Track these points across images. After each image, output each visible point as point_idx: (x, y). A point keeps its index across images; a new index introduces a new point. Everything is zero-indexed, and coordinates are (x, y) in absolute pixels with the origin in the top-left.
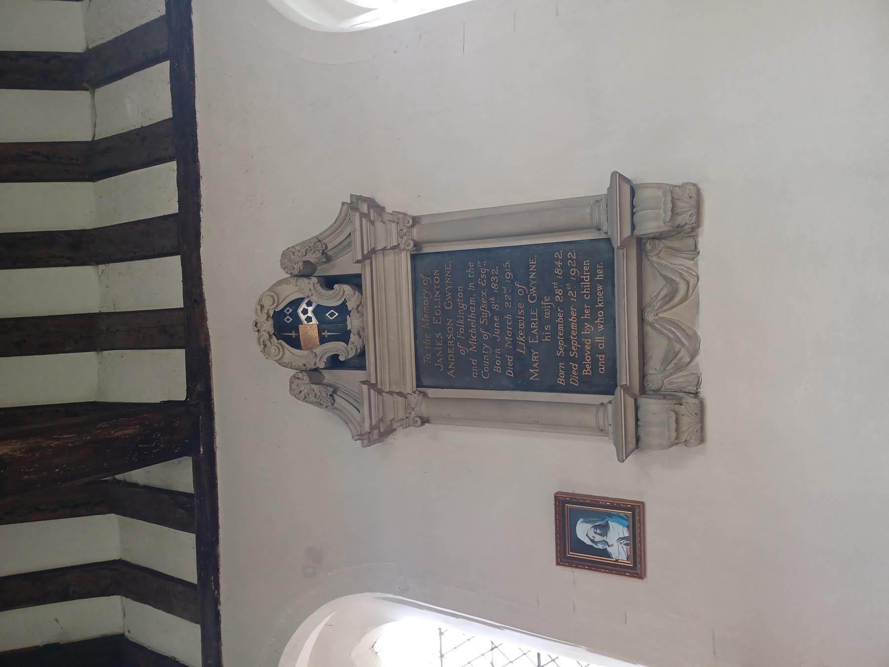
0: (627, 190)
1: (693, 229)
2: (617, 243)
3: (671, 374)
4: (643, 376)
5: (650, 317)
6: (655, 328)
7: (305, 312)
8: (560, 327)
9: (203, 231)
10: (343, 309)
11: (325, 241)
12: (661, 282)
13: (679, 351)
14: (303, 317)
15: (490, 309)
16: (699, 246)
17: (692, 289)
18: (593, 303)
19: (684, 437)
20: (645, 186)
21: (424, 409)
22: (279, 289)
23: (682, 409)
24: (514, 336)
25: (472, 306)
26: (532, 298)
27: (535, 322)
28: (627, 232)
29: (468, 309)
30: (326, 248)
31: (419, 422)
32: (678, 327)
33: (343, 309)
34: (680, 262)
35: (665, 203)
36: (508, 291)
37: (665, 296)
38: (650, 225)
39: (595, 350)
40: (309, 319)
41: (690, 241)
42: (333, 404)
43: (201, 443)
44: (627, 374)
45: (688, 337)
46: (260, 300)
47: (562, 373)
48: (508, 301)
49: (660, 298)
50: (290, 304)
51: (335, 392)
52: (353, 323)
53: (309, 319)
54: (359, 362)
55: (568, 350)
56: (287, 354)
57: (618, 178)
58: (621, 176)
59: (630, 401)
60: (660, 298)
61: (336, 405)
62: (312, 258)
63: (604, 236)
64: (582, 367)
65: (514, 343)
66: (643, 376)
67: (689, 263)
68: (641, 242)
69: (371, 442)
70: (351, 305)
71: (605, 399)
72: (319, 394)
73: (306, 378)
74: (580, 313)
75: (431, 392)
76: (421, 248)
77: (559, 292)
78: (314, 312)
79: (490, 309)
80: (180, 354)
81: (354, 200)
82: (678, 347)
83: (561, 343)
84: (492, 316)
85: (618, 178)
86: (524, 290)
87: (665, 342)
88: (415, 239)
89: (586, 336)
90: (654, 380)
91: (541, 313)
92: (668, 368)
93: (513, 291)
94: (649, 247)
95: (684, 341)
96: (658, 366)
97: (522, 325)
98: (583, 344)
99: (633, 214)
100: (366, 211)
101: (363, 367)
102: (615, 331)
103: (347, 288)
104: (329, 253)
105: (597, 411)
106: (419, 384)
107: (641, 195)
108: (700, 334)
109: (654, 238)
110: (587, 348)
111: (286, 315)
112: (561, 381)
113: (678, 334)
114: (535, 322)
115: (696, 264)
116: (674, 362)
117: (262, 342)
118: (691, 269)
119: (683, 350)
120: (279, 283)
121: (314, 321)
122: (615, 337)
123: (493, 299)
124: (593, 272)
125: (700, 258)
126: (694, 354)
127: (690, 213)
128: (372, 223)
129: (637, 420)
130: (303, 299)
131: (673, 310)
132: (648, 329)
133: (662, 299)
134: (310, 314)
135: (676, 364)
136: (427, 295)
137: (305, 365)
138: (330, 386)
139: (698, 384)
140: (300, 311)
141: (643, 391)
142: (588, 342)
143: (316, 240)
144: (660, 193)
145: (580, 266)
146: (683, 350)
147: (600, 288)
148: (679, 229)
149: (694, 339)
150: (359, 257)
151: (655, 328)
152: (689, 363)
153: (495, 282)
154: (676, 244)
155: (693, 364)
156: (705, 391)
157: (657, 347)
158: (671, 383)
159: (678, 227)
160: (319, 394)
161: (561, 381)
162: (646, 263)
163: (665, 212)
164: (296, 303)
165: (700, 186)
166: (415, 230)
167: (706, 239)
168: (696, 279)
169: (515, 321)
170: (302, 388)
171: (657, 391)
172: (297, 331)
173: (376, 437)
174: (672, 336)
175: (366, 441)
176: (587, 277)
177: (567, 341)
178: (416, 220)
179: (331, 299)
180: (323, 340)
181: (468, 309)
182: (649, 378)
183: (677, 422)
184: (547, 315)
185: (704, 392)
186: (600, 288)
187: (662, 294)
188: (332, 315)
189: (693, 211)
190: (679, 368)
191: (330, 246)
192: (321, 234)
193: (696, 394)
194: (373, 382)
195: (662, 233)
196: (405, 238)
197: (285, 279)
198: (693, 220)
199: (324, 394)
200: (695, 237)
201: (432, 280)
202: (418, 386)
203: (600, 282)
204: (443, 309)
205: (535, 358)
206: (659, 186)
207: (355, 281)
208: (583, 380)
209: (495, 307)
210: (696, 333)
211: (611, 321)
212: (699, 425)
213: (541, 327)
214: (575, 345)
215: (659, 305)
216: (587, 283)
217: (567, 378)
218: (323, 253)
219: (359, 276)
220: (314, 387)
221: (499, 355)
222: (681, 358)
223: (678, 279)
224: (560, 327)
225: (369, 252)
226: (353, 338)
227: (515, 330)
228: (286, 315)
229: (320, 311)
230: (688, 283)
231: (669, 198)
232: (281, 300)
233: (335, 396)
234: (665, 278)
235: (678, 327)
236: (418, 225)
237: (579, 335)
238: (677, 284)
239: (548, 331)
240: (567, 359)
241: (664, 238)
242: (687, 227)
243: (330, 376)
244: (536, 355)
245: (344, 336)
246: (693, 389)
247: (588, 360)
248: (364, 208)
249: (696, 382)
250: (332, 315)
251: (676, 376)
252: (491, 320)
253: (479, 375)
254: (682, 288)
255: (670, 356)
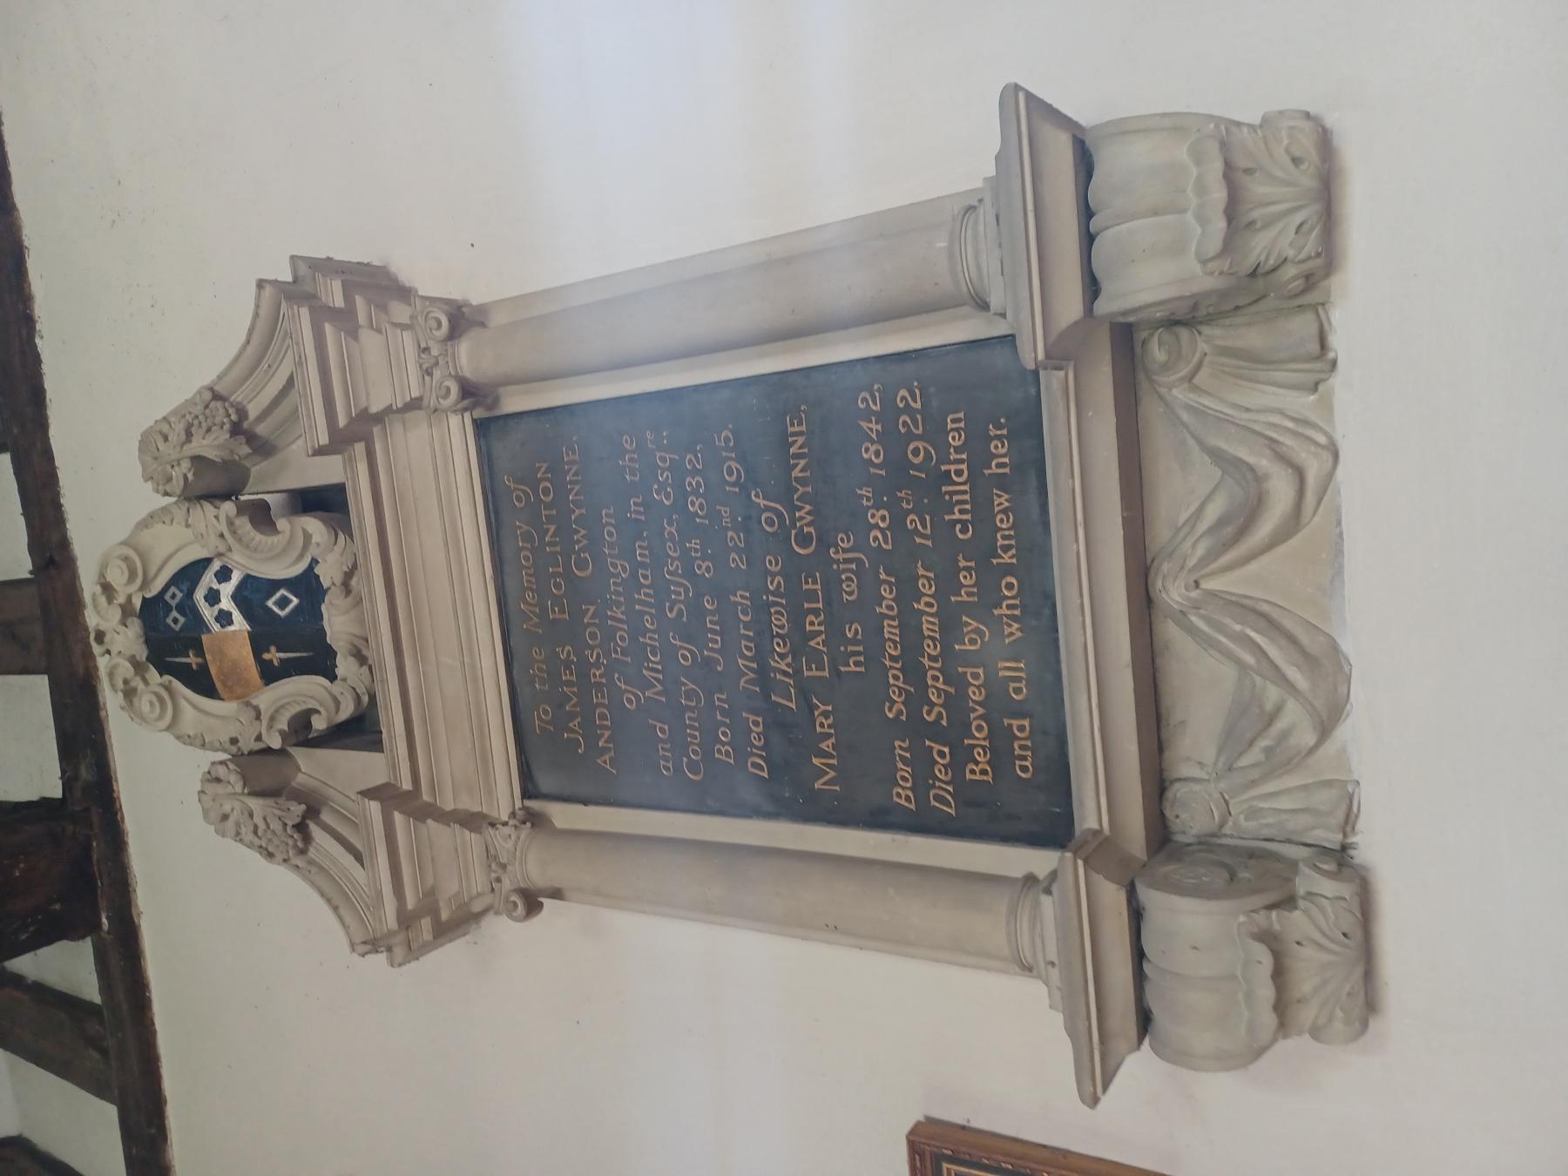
0: (1060, 157)
1: (1311, 281)
2: (1032, 351)
3: (1254, 783)
4: (1158, 784)
5: (1172, 592)
6: (1192, 630)
7: (213, 597)
8: (890, 630)
9: (49, 384)
10: (308, 586)
11: (237, 397)
12: (1204, 474)
13: (1279, 709)
14: (208, 613)
15: (690, 574)
16: (1334, 340)
17: (1312, 497)
18: (984, 552)
19: (1307, 1015)
20: (1123, 129)
21: (537, 866)
22: (146, 537)
23: (1296, 923)
24: (761, 657)
25: (643, 565)
26: (804, 540)
27: (816, 612)
28: (1070, 306)
29: (634, 575)
30: (242, 413)
31: (521, 910)
32: (1271, 625)
33: (308, 586)
34: (1273, 400)
35: (1201, 189)
36: (734, 520)
37: (1221, 523)
38: (1146, 278)
39: (998, 704)
40: (224, 618)
41: (1302, 325)
42: (303, 852)
43: (103, 904)
44: (1103, 796)
45: (1308, 660)
46: (102, 575)
47: (904, 771)
48: (736, 548)
49: (1202, 527)
50: (175, 580)
51: (312, 812)
52: (337, 623)
53: (224, 618)
54: (360, 730)
55: (917, 699)
56: (188, 713)
57: (1027, 112)
58: (1030, 97)
59: (1112, 896)
60: (1202, 527)
61: (312, 853)
62: (209, 445)
63: (1001, 329)
64: (961, 757)
65: (763, 675)
66: (1158, 784)
67: (1302, 403)
68: (1125, 338)
69: (414, 952)
70: (328, 574)
71: (1040, 861)
72: (262, 826)
73: (233, 778)
74: (947, 583)
75: (562, 815)
76: (496, 401)
77: (880, 518)
78: (237, 597)
79: (690, 574)
80: (41, 683)
81: (303, 269)
82: (1273, 693)
83: (896, 681)
84: (699, 596)
85: (1027, 112)
86: (780, 515)
87: (1229, 672)
88: (467, 373)
89: (968, 659)
90: (1193, 814)
91: (832, 586)
92: (1244, 762)
93: (747, 518)
94: (1157, 353)
95: (1294, 674)
96: (1209, 753)
97: (780, 623)
98: (961, 684)
99: (1088, 239)
100: (339, 302)
101: (376, 745)
102: (1056, 640)
103: (313, 525)
104: (261, 430)
105: (1013, 912)
106: (529, 790)
107: (1112, 163)
108: (1346, 646)
109: (1172, 323)
110: (975, 695)
111: (169, 609)
112: (903, 796)
113: (1273, 652)
114: (816, 612)
115: (1327, 406)
116: (1264, 742)
117: (120, 685)
118: (1306, 422)
119: (1292, 706)
120: (144, 524)
121: (239, 623)
122: (1058, 662)
123: (694, 544)
124: (979, 458)
125: (1337, 381)
126: (1328, 719)
127: (1298, 218)
128: (353, 333)
129: (1139, 955)
130: (207, 562)
131: (1253, 567)
132: (1170, 631)
133: (1211, 530)
134: (226, 604)
135: (1268, 751)
136: (528, 537)
137: (234, 741)
138: (298, 795)
139: (1349, 822)
140: (199, 595)
141: (1161, 836)
142: (975, 677)
143: (208, 396)
144: (1182, 153)
145: (935, 434)
146: (1292, 706)
147: (1002, 500)
148: (1260, 284)
149: (1328, 666)
150: (324, 439)
151: (1192, 630)
152: (1312, 750)
153: (695, 492)
154: (1252, 337)
155: (1330, 747)
156: (1374, 846)
157: (1204, 689)
158: (1253, 813)
159: (1253, 274)
160: (262, 826)
161: (903, 796)
162: (1151, 410)
163: (1202, 220)
164: (190, 574)
165: (1330, 121)
166: (464, 348)
167: (1358, 310)
168: (1327, 456)
169: (762, 610)
170: (227, 808)
171: (1207, 843)
172: (200, 652)
173: (427, 936)
174: (1249, 659)
175: (399, 952)
176: (958, 468)
177: (914, 672)
178: (462, 319)
179: (276, 557)
180: (271, 675)
181: (634, 575)
182: (1178, 791)
183: (1279, 974)
184: (850, 590)
185: (1371, 847)
186: (1002, 500)
187: (1213, 512)
188: (283, 602)
189: (1310, 213)
190: (1281, 761)
191: (253, 410)
192: (220, 377)
193: (1341, 859)
194: (407, 785)
195: (1195, 302)
196: (437, 374)
197: (164, 509)
198: (1311, 244)
199: (276, 825)
200: (1318, 309)
201: (536, 494)
202: (526, 795)
203: (1002, 483)
204: (568, 575)
205: (823, 724)
206: (1175, 125)
207: (325, 502)
208: (967, 795)
209: (703, 569)
210: (1335, 648)
211: (1040, 609)
212: (1359, 971)
213: (835, 632)
214: (936, 689)
215: (1201, 550)
216: (960, 487)
217: (922, 783)
218: (236, 429)
219: (340, 489)
220: (255, 804)
221: (724, 712)
222: (1285, 735)
223: (1264, 463)
224: (890, 630)
225: (351, 421)
226: (345, 665)
227: (763, 634)
228: (169, 609)
229: (252, 594)
230: (1300, 474)
231: (1218, 166)
232: (153, 570)
233: (314, 829)
234: (1217, 456)
235: (1271, 625)
236: (474, 333)
237: (947, 654)
238: (1260, 479)
239: (854, 642)
240: (916, 729)
241: (1210, 320)
242: (1290, 271)
243: (312, 766)
244: (826, 714)
245: (321, 662)
246: (1332, 839)
247: (980, 736)
248: (334, 295)
249: (1340, 815)
250: (283, 602)
251: (1271, 787)
252: (697, 612)
253: (678, 770)
254: (1281, 490)
255: (1248, 723)
